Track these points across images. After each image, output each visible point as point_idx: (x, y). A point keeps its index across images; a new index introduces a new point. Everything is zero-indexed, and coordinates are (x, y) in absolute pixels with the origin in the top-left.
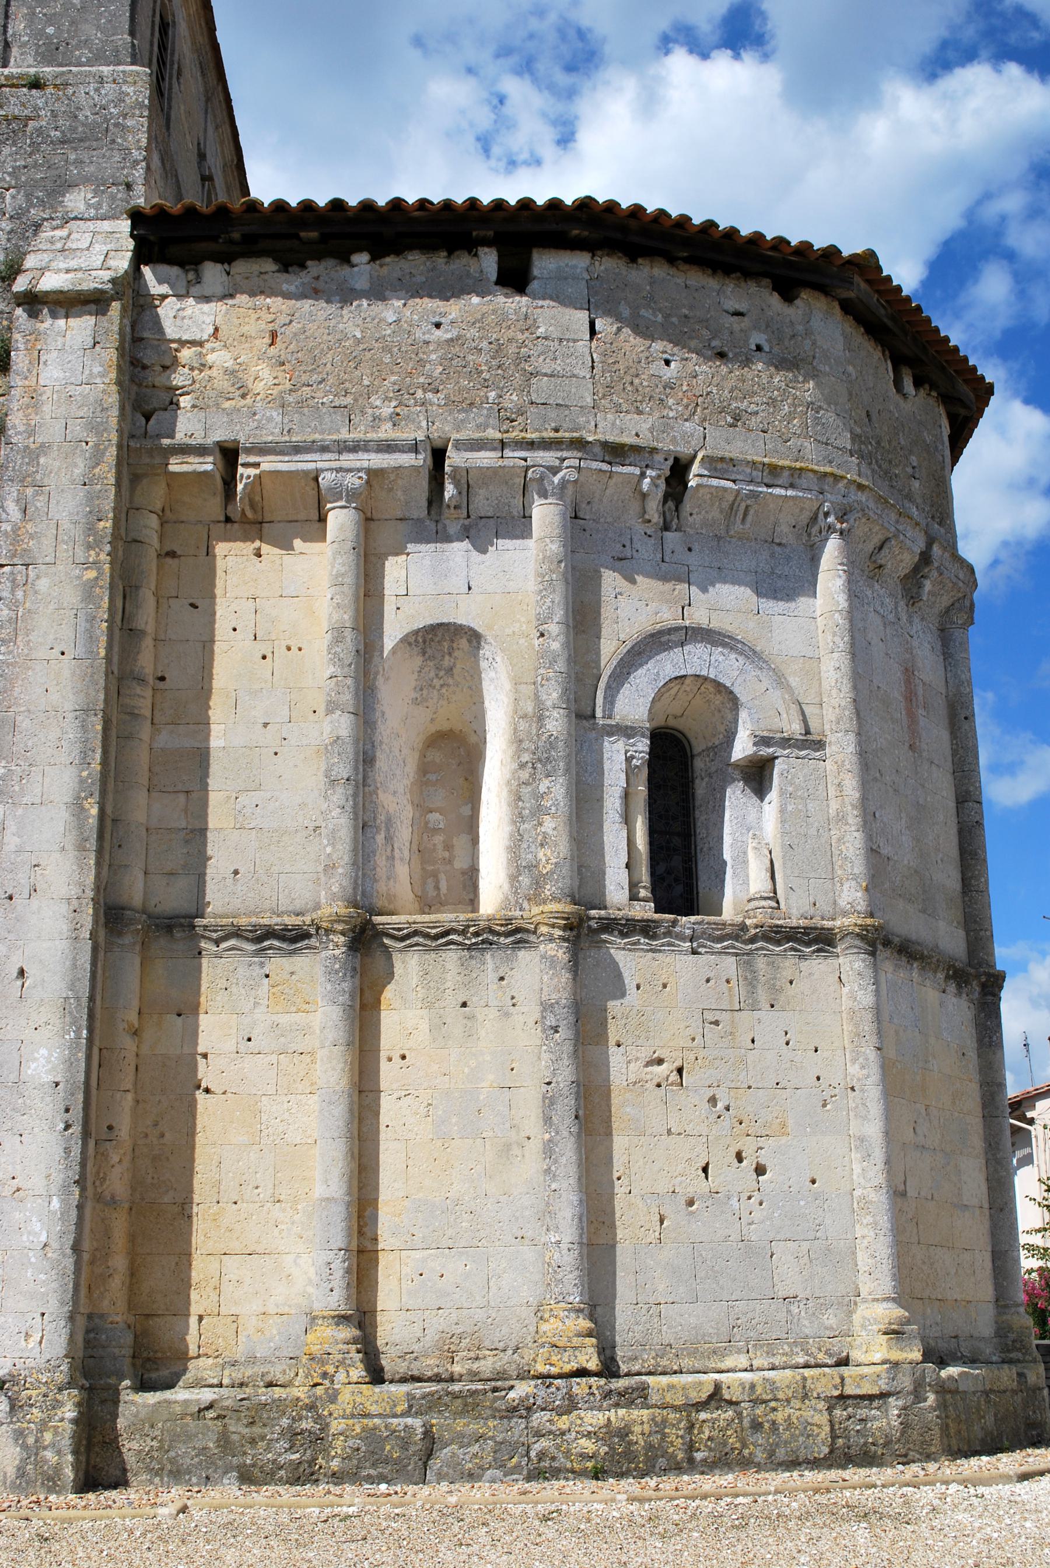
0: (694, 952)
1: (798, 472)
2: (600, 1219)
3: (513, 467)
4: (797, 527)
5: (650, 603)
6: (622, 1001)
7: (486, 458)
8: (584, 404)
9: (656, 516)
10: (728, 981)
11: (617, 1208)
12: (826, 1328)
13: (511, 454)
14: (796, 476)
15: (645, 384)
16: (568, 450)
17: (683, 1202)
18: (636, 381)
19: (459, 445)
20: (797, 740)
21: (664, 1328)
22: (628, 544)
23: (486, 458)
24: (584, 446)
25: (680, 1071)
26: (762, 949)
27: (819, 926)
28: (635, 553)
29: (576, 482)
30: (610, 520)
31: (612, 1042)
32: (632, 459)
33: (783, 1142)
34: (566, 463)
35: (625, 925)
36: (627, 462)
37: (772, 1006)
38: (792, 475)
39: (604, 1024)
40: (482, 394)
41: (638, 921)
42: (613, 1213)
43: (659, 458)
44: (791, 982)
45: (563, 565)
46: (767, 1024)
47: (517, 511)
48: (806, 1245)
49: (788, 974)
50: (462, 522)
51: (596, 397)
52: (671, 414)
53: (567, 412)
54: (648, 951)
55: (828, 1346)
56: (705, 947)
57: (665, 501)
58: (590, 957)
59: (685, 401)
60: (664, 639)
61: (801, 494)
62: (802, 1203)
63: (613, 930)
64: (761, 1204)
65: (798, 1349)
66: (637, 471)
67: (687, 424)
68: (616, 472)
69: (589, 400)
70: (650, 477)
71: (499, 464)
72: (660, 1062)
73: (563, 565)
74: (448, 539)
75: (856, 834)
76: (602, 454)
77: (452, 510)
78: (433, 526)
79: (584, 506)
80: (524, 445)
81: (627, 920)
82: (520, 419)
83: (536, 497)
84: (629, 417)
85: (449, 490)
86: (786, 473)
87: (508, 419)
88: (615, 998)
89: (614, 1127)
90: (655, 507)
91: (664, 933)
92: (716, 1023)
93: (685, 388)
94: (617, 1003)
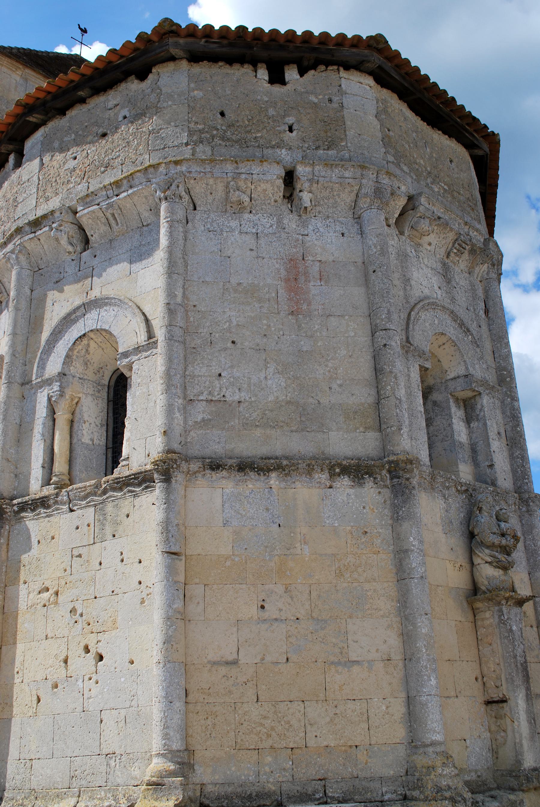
0: (72, 511)
1: (131, 177)
2: (5, 702)
4: (152, 209)
5: (69, 300)
6: (29, 554)
10: (89, 525)
11: (15, 693)
12: (132, 778)
14: (131, 180)
17: (50, 686)
20: (143, 346)
21: (32, 777)
24: (21, 231)
25: (57, 593)
26: (111, 497)
27: (143, 470)
30: (53, 262)
31: (22, 582)
33: (113, 634)
35: (32, 504)
37: (114, 536)
38: (129, 181)
39: (18, 571)
41: (38, 499)
42: (12, 697)
44: (128, 516)
46: (110, 549)
48: (123, 712)
49: (125, 511)
54: (46, 517)
55: (131, 793)
56: (77, 505)
58: (16, 529)
60: (72, 317)
61: (136, 189)
62: (123, 680)
63: (27, 509)
64: (97, 683)
65: (109, 795)
72: (47, 590)
75: (161, 397)
81: (32, 500)
86: (125, 182)
88: (25, 552)
89: (18, 638)
91: (54, 503)
92: (80, 556)
94: (26, 556)
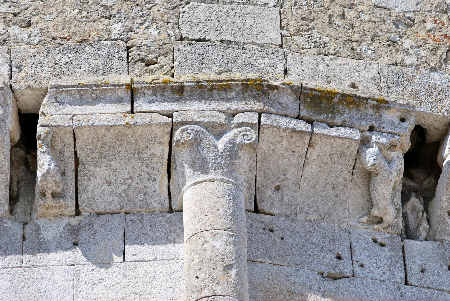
3: (150, 125)
7: (107, 113)
8: (266, 40)
9: (391, 211)
13: (146, 107)
15: (365, 17)
16: (239, 99)
18: (350, 14)
19: (61, 94)
22: (346, 255)
23: (107, 113)
24: (266, 94)
28: (358, 270)
29: (253, 146)
30: (313, 217)
32: (346, 116)
34: (238, 119)
36: (339, 122)
40: (101, 26)
43: (391, 116)
45: (233, 272)
47: (158, 198)
50: (66, 220)
51: (285, 32)
52: (408, 60)
53: (238, 52)
57: (405, 198)
59: (431, 42)
66: (356, 135)
67: (436, 75)
68: (321, 135)
69: (274, 36)
70: (378, 143)
71: (127, 120)
73: (233, 272)
74: (42, 247)
76: (296, 106)
77: (49, 201)
78: (18, 229)
79: (269, 193)
80: (168, 93)
82: (162, 60)
83: (188, 172)
84: (339, 61)
85: (44, 161)
87: (142, 60)
90: (388, 196)
93: (429, 25)
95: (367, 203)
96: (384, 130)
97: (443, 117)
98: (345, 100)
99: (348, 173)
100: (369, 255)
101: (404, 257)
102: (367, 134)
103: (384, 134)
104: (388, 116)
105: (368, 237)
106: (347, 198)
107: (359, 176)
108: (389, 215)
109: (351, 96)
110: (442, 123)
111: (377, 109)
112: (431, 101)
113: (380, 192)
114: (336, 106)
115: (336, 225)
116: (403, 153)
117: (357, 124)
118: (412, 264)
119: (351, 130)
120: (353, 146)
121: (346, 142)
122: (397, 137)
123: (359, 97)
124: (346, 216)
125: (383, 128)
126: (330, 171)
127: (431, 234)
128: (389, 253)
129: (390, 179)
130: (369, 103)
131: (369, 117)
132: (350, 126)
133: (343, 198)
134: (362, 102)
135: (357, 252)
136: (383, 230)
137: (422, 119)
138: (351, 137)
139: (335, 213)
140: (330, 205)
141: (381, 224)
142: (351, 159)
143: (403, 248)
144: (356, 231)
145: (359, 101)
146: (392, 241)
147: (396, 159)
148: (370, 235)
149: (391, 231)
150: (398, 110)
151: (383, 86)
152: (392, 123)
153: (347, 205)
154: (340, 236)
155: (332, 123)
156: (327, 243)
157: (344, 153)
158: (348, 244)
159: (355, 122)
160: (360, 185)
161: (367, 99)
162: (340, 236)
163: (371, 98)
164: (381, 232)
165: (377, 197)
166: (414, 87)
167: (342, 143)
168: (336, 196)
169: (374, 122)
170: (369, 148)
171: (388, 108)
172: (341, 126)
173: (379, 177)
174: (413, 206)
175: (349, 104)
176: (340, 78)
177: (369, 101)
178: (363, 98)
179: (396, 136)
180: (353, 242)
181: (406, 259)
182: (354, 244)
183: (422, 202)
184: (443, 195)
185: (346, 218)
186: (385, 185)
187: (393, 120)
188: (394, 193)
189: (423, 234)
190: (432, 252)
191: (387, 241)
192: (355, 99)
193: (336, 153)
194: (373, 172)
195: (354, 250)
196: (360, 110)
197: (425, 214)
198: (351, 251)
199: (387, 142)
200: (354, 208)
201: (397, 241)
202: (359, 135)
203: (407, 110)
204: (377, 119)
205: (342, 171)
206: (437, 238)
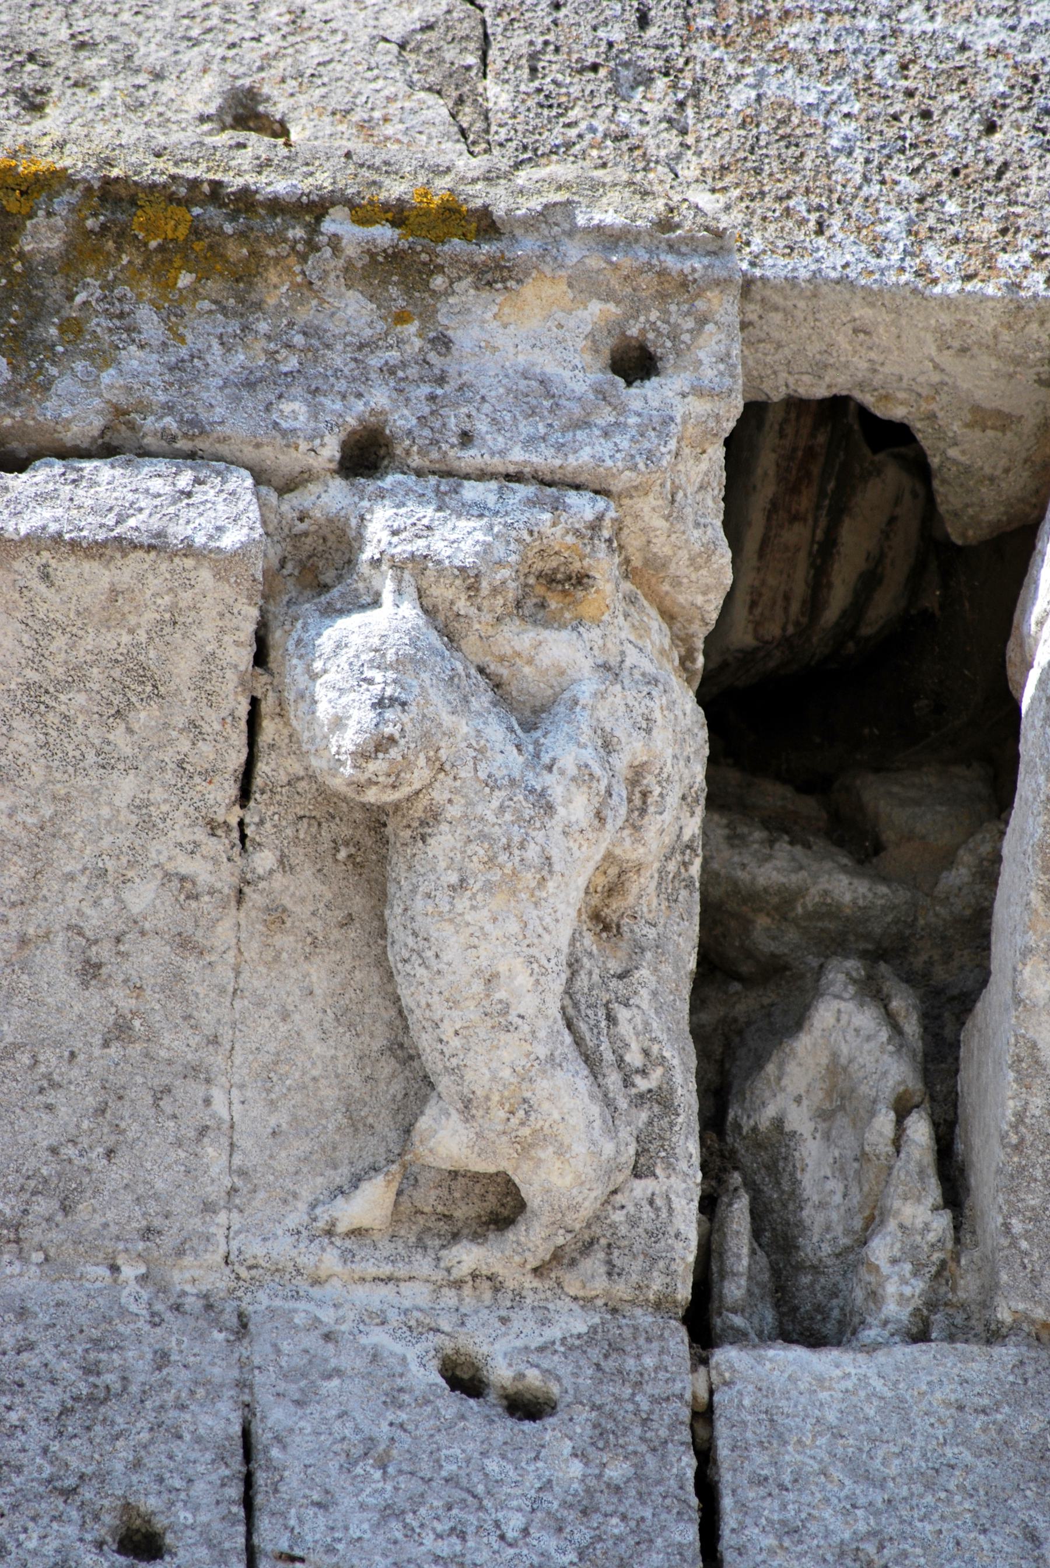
32: (139, 366)
43: (529, 337)
66: (226, 515)
70: (416, 566)
95: (387, 1067)
96: (470, 458)
97: (1018, 309)
98: (123, 236)
99: (200, 834)
100: (401, 1502)
101: (707, 1489)
102: (333, 496)
103: (471, 491)
104: (502, 339)
105: (398, 1348)
106: (214, 1041)
107: (297, 856)
108: (561, 1152)
109: (172, 198)
110: (1018, 361)
111: (408, 291)
112: (912, 186)
113: (465, 972)
114: (54, 287)
115: (129, 1272)
116: (681, 639)
117: (233, 423)
118: (770, 1541)
119: (185, 480)
120: (209, 611)
121: (151, 582)
122: (583, 507)
123: (245, 201)
124: (215, 1192)
125: (466, 438)
126: (48, 831)
127: (968, 1287)
128: (576, 1468)
129: (532, 852)
130: (335, 242)
131: (338, 358)
132: (182, 444)
133: (177, 1043)
134: (274, 240)
135: (293, 1478)
136: (530, 1282)
137: (842, 341)
138: (178, 531)
139: (117, 1174)
140: (71, 1109)
141: (510, 1235)
142: (211, 715)
143: (704, 1415)
144: (302, 1312)
145: (242, 235)
146: (609, 1365)
147: (586, 690)
148: (416, 1329)
149: (600, 1284)
150: (587, 286)
151: (497, 95)
152: (538, 394)
153: (218, 1096)
154: (162, 1359)
155: (20, 431)
156: (38, 1432)
157: (143, 674)
158: (221, 1421)
159: (213, 403)
160: (317, 926)
161: (313, 209)
162: (162, 1359)
163: (349, 203)
164: (519, 1296)
165: (440, 1010)
166: (771, 88)
167: (114, 593)
168: (120, 1031)
169: (380, 397)
170: (332, 612)
171: (495, 276)
172: (106, 450)
173: (443, 842)
174: (836, 1070)
175: (159, 264)
176: (127, 63)
177: (336, 223)
178: (276, 206)
179: (572, 498)
180: (264, 1397)
181: (727, 1502)
182: (275, 1415)
183: (912, 1027)
184: (1027, 952)
185: (208, 1208)
186: (498, 902)
187: (551, 369)
188: (614, 966)
189: (891, 1288)
190: (959, 1436)
191: (565, 1370)
192: (213, 215)
193: (76, 677)
194: (397, 806)
195: (271, 1467)
196: (258, 306)
197: (920, 1130)
198: (248, 1481)
199: (499, 551)
200: (281, 1118)
201: (649, 1361)
202: (254, 513)
203: (663, 273)
204: (413, 372)
205: (147, 826)
206: (1004, 1315)
